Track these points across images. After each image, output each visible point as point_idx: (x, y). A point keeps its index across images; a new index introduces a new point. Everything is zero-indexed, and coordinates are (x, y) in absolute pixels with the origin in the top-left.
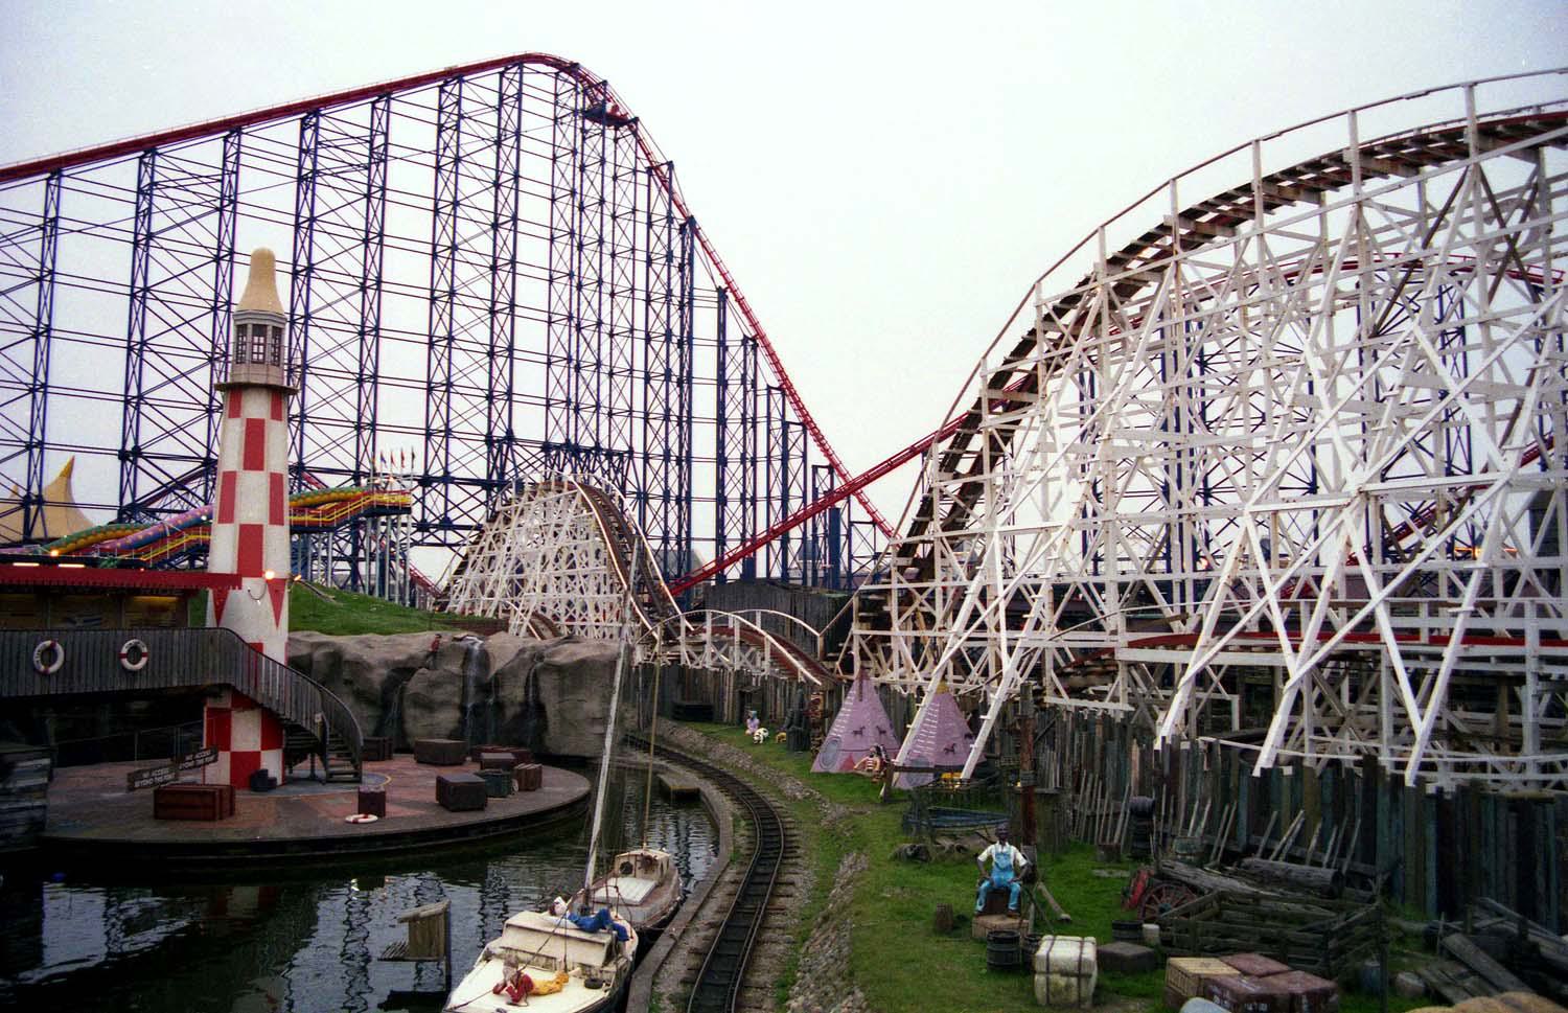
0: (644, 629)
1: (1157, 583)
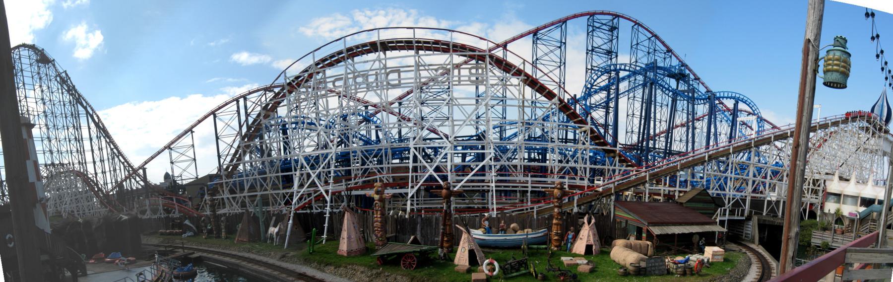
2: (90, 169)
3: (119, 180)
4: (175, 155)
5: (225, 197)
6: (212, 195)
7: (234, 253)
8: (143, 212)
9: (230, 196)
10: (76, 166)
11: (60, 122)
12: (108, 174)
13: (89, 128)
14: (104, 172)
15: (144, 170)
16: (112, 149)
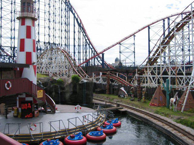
0: (73, 69)
1: (126, 80)
2: (71, 50)
3: (88, 58)
4: (122, 48)
5: (148, 76)
6: (141, 74)
7: (148, 112)
8: (97, 80)
9: (151, 76)
10: (63, 46)
11: (58, 19)
12: (82, 54)
13: (74, 26)
14: (79, 53)
15: (103, 55)
16: (86, 40)
